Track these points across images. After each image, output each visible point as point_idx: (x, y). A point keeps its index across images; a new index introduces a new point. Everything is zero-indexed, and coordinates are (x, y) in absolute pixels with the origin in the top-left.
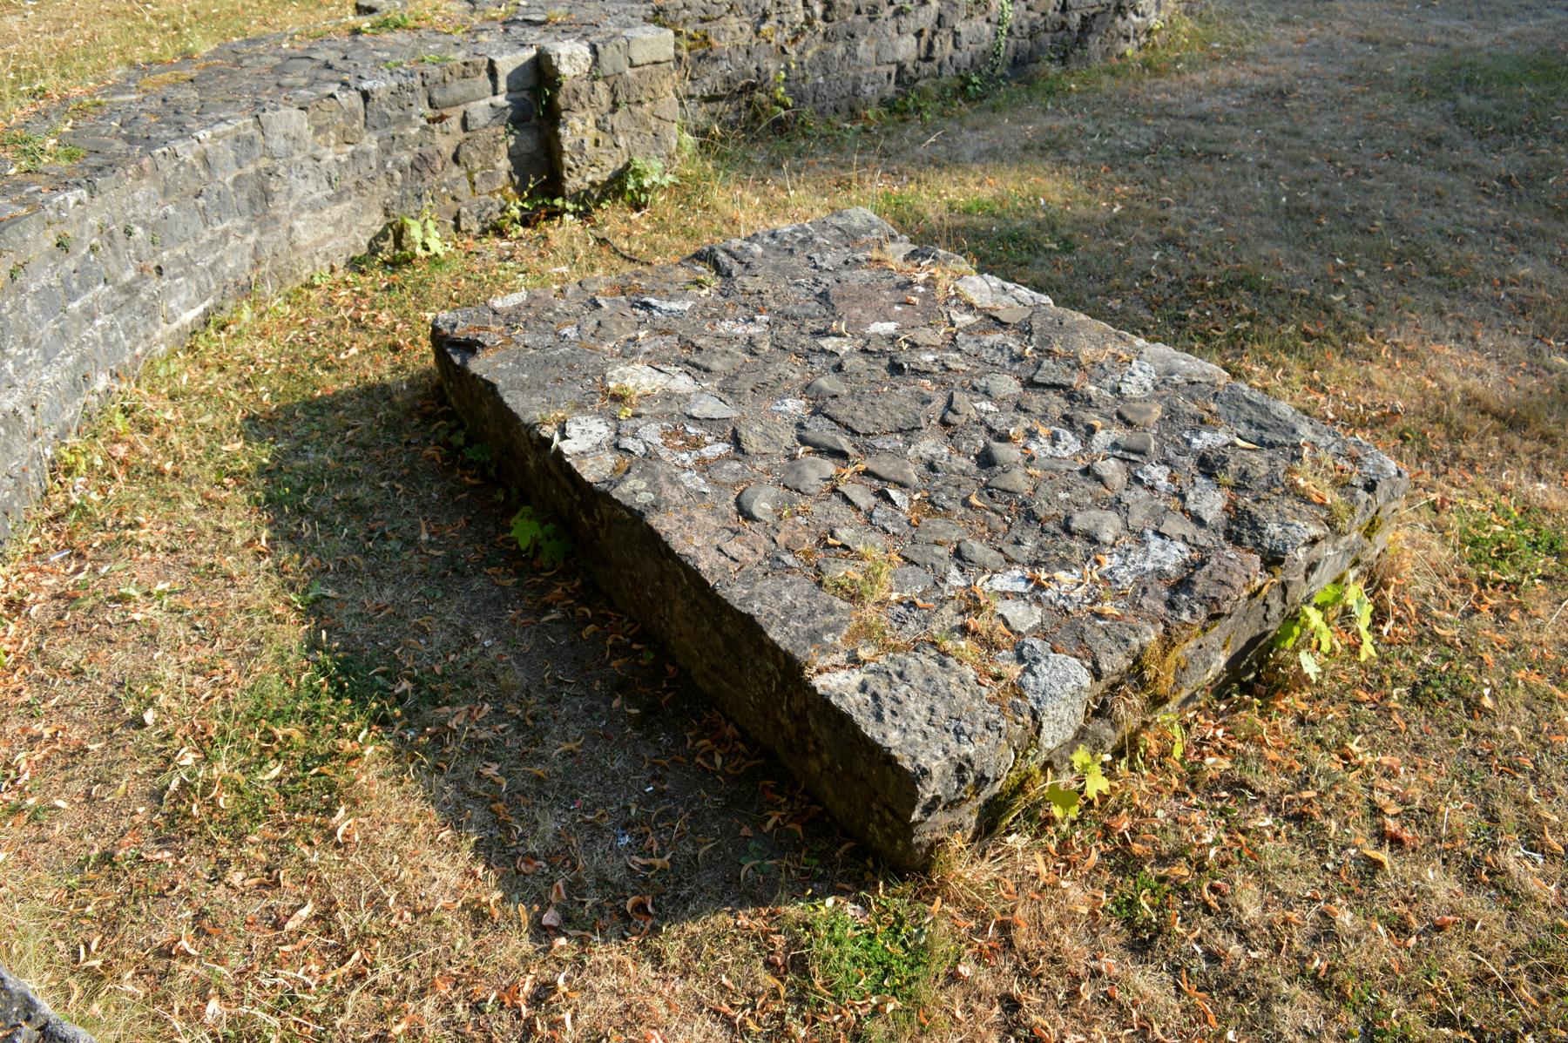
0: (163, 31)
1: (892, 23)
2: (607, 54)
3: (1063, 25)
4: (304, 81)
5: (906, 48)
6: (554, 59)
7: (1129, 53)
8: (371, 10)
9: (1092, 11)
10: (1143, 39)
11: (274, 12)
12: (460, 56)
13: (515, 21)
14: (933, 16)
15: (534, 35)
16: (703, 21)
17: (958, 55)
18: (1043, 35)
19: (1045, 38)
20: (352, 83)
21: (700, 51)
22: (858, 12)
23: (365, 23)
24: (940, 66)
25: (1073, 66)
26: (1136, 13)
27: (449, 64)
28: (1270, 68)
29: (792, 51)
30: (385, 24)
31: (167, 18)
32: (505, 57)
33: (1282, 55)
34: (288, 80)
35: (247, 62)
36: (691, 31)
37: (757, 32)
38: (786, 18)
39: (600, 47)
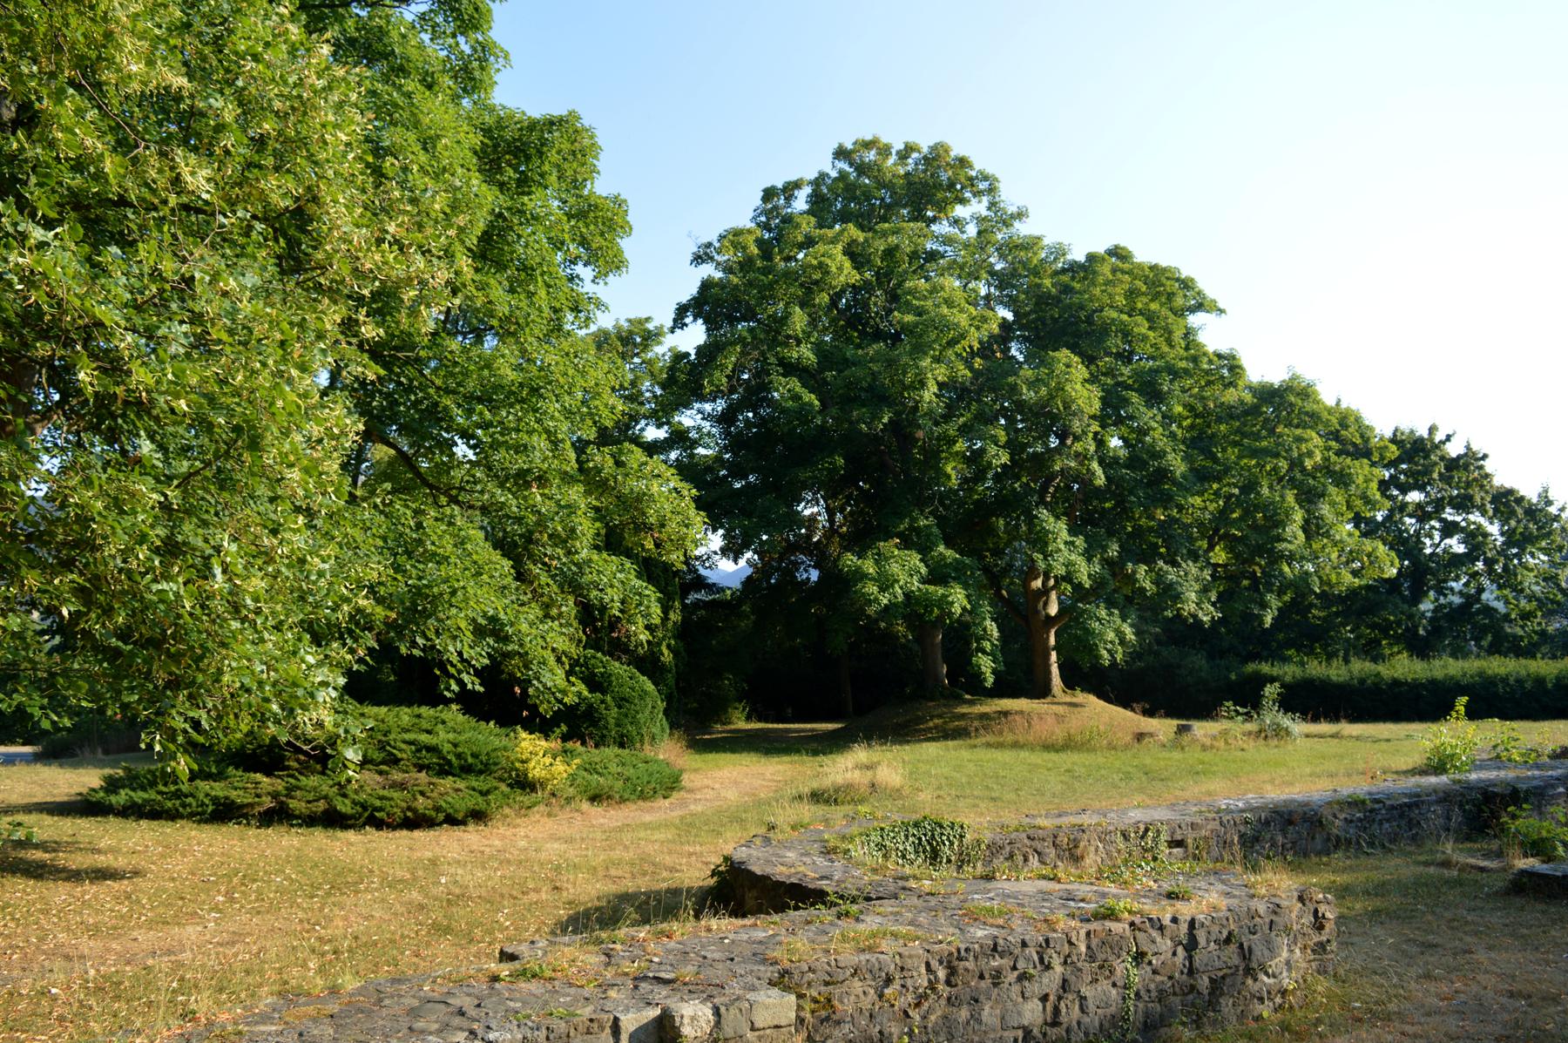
0: (323, 955)
1: (1016, 988)
2: (730, 1016)
3: (1193, 988)
4: (436, 1026)
5: (1032, 1013)
6: (677, 1020)
7: (1265, 1014)
8: (512, 957)
9: (1220, 974)
10: (1278, 1000)
11: (428, 944)
12: (587, 1011)
13: (645, 978)
14: (1058, 981)
15: (661, 993)
16: (827, 984)
17: (1086, 1020)
18: (1172, 998)
19: (1176, 1001)
20: (480, 1032)
21: (824, 1014)
22: (982, 977)
23: (505, 970)
24: (1068, 1031)
25: (1208, 1030)
26: (1268, 975)
27: (575, 1020)
28: (1417, 1029)
29: (915, 1015)
30: (523, 973)
31: (330, 941)
32: (630, 1016)
33: (1428, 1014)
34: (420, 1025)
35: (387, 1002)
36: (815, 994)
37: (881, 996)
38: (909, 982)
39: (723, 1009)
